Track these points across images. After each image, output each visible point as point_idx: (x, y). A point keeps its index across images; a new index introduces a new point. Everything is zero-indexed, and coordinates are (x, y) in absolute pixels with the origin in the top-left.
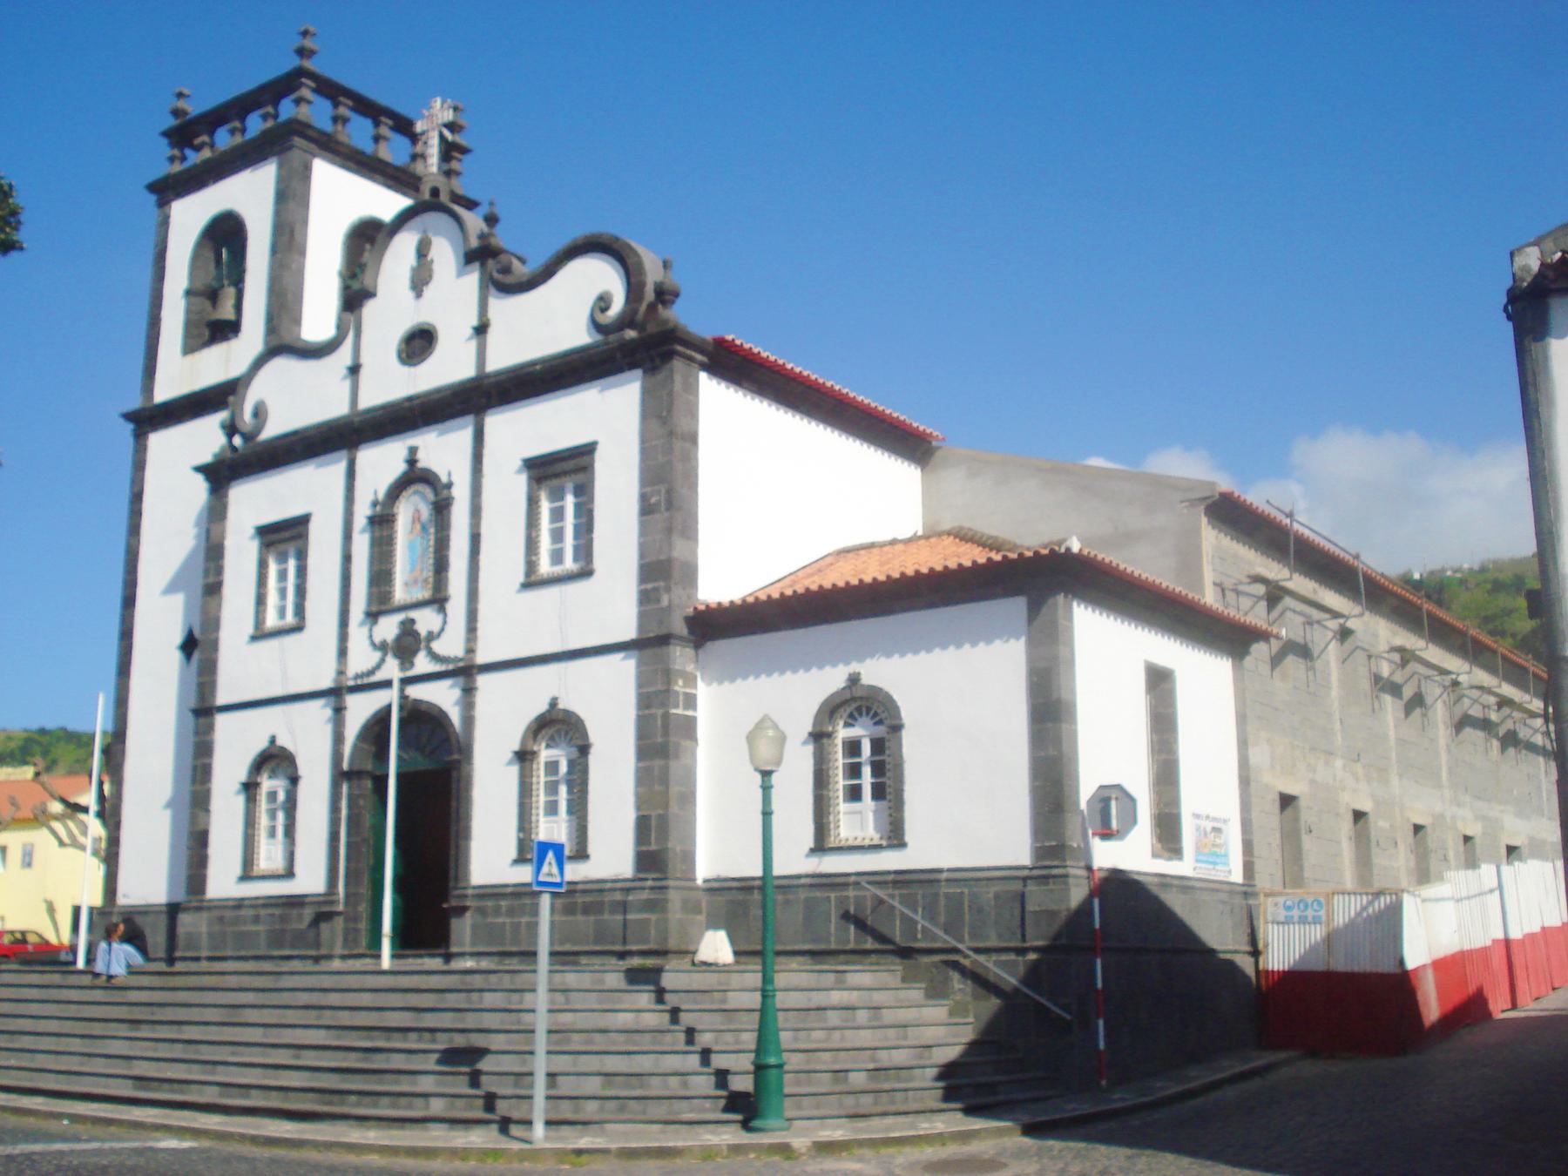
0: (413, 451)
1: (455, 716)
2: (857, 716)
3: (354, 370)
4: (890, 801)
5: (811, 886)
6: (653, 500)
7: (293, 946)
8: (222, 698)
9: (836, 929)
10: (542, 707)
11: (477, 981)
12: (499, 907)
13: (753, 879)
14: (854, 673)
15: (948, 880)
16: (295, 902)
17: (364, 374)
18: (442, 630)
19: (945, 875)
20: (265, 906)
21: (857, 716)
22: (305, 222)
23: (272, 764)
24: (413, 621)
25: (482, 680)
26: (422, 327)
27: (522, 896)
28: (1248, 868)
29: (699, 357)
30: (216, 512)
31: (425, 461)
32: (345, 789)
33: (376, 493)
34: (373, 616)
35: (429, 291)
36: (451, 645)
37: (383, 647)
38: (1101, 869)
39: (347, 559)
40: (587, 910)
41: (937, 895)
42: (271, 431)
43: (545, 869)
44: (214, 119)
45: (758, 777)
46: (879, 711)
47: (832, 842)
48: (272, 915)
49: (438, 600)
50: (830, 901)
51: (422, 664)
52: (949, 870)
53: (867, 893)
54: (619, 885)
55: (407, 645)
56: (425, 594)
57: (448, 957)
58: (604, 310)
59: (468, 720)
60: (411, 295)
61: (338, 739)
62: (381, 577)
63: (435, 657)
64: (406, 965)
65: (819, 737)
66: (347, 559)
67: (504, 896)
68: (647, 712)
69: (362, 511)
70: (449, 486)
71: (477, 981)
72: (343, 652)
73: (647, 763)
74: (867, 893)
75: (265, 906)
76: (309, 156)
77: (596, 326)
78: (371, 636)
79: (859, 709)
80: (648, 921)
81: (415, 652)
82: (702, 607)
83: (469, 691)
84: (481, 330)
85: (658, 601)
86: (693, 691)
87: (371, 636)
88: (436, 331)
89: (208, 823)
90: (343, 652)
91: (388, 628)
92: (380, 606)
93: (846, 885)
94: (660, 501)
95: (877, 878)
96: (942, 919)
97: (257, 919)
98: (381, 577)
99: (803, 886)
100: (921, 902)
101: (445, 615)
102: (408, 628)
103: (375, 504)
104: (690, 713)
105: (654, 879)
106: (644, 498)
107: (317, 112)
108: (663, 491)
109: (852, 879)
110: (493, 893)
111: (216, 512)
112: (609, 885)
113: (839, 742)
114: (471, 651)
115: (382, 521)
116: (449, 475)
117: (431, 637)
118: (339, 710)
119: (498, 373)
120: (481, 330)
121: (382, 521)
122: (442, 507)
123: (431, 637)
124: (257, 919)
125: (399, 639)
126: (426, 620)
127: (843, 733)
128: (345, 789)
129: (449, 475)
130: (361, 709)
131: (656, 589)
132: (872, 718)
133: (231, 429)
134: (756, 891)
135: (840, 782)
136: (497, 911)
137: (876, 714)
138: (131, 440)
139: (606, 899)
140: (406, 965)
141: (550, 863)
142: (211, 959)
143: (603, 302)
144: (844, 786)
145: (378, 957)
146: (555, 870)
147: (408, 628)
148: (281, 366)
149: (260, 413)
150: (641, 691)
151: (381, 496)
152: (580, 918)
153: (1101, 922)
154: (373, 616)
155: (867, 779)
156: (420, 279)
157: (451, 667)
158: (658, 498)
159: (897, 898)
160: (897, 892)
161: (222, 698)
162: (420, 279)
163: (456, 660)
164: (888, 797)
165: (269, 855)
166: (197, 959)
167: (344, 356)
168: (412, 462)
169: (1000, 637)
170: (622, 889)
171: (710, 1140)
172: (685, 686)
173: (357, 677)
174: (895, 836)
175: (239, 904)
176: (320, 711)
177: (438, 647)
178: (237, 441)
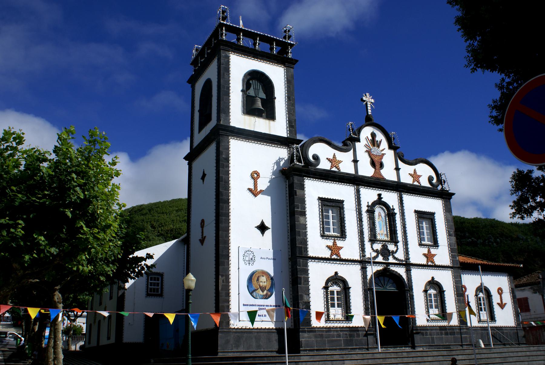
1: (404, 276)
7: (356, 345)
11: (424, 354)
12: (442, 332)
28: (222, 359)
33: (368, 203)
37: (377, 251)
38: (219, 316)
48: (346, 334)
49: (394, 239)
51: (391, 260)
55: (385, 252)
57: (413, 347)
64: (397, 350)
65: (326, 288)
69: (364, 208)
71: (424, 354)
73: (459, 298)
80: (467, 337)
83: (408, 271)
91: (378, 246)
92: (373, 240)
93: (428, 329)
101: (397, 247)
115: (371, 211)
116: (393, 206)
121: (371, 211)
124: (339, 336)
125: (381, 250)
126: (391, 247)
129: (393, 206)
130: (371, 270)
136: (426, 334)
139: (455, 331)
140: (397, 350)
142: (317, 350)
147: (385, 248)
151: (370, 204)
157: (397, 262)
166: (313, 350)
169: (472, 219)
176: (357, 268)
177: (396, 255)
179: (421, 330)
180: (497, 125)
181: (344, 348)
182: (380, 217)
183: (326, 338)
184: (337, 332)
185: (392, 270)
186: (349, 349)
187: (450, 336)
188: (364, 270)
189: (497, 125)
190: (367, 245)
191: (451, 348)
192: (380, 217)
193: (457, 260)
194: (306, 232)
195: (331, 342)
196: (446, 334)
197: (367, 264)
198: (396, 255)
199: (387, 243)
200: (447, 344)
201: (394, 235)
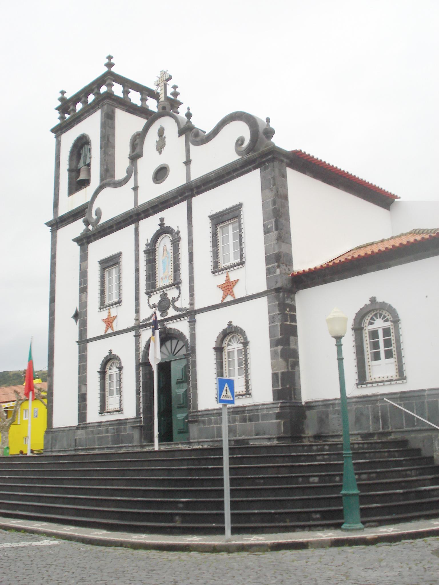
0: (162, 220)
1: (187, 333)
2: (373, 321)
3: (135, 189)
4: (395, 358)
5: (356, 402)
6: (269, 227)
8: (89, 336)
9: (372, 422)
10: (225, 326)
13: (336, 399)
14: (372, 297)
15: (428, 395)
16: (121, 423)
17: (139, 191)
18: (179, 297)
19: (426, 393)
20: (110, 425)
21: (373, 321)
22: (114, 135)
23: (110, 363)
24: (166, 294)
25: (198, 317)
26: (162, 166)
27: (218, 413)
29: (285, 160)
30: (84, 257)
31: (167, 224)
32: (141, 369)
34: (149, 294)
35: (164, 151)
36: (184, 303)
37: (154, 306)
39: (137, 270)
40: (251, 420)
41: (423, 402)
42: (103, 220)
43: (224, 393)
44: (76, 99)
45: (334, 341)
46: (386, 315)
47: (368, 380)
48: (114, 429)
49: (176, 283)
50: (368, 409)
51: (171, 312)
52: (429, 390)
53: (387, 404)
54: (265, 406)
56: (170, 281)
58: (242, 144)
59: (193, 336)
60: (157, 153)
61: (137, 349)
62: (152, 276)
63: (176, 309)
65: (358, 329)
66: (137, 270)
67: (213, 415)
68: (273, 324)
69: (143, 247)
70: (178, 233)
72: (137, 311)
74: (387, 404)
75: (110, 425)
76: (113, 107)
77: (239, 153)
78: (148, 303)
79: (376, 315)
81: (168, 308)
82: (296, 273)
83: (192, 323)
84: (188, 162)
85: (275, 272)
86: (294, 313)
87: (148, 303)
88: (169, 168)
89: (86, 391)
90: (137, 311)
91: (156, 299)
92: (152, 288)
94: (272, 226)
95: (392, 396)
96: (427, 414)
97: (107, 431)
98: (152, 276)
99: (353, 402)
100: (415, 407)
101: (180, 290)
102: (164, 296)
103: (147, 245)
104: (293, 324)
105: (281, 403)
106: (265, 226)
107: (118, 90)
108: (273, 222)
109: (379, 397)
110: (209, 413)
111: (84, 257)
112: (260, 407)
113: (367, 331)
114: (192, 304)
117: (174, 300)
118: (137, 336)
119: (196, 181)
120: (188, 162)
122: (176, 243)
123: (174, 300)
124: (107, 431)
126: (172, 293)
127: (368, 328)
128: (141, 369)
131: (273, 267)
132: (383, 319)
133: (87, 223)
134: (331, 406)
135: (368, 351)
137: (384, 317)
138: (50, 234)
141: (226, 390)
143: (240, 142)
144: (371, 352)
145: (153, 445)
146: (229, 394)
147: (164, 296)
148: (107, 191)
149: (99, 213)
150: (271, 339)
152: (248, 423)
153: (284, 429)
154: (149, 294)
155: (382, 349)
156: (160, 146)
157: (178, 313)
158: (271, 225)
159: (403, 406)
160: (402, 403)
161: (89, 336)
162: (160, 146)
163: (185, 309)
164: (394, 356)
165: (112, 403)
167: (131, 183)
168: (162, 224)
170: (267, 408)
171: (321, 537)
172: (289, 311)
173: (144, 321)
174: (401, 376)
175: (100, 424)
177: (177, 304)
178: (90, 227)
179: (203, 416)
180: (155, 304)
181: (111, 446)
182: (165, 252)
183: (96, 434)
184: (106, 427)
185: (170, 328)
186: (114, 447)
187: (249, 423)
188: (137, 336)
189: (155, 304)
190: (143, 297)
191: (249, 444)
192: (165, 252)
193: (277, 276)
194: (86, 311)
195: (100, 438)
196: (244, 420)
197: (165, 323)
198: (177, 304)
199: (165, 290)
200: (243, 437)
201: (247, 409)
